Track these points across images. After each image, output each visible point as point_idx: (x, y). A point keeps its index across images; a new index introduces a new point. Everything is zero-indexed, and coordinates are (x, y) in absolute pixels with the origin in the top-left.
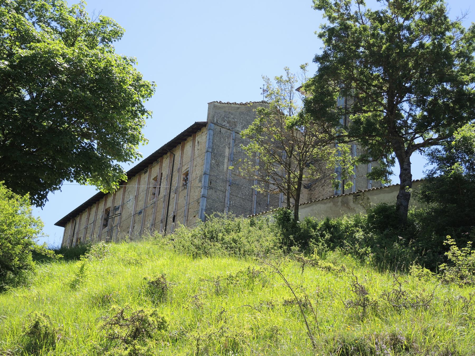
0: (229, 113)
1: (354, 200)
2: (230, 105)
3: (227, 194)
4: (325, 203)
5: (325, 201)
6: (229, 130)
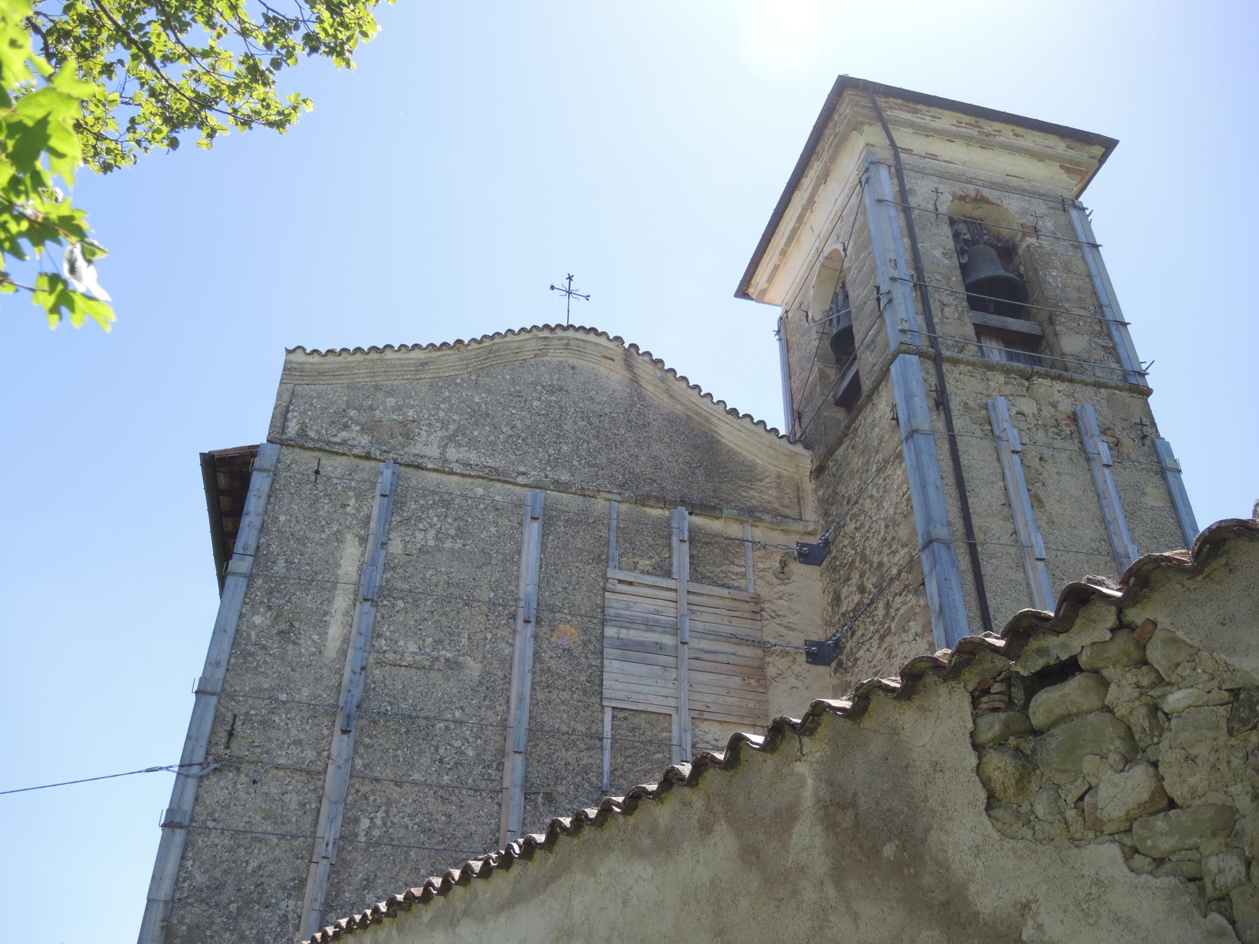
0: (377, 388)
1: (1000, 765)
2: (374, 356)
3: (333, 781)
4: (666, 846)
5: (663, 813)
6: (367, 457)
